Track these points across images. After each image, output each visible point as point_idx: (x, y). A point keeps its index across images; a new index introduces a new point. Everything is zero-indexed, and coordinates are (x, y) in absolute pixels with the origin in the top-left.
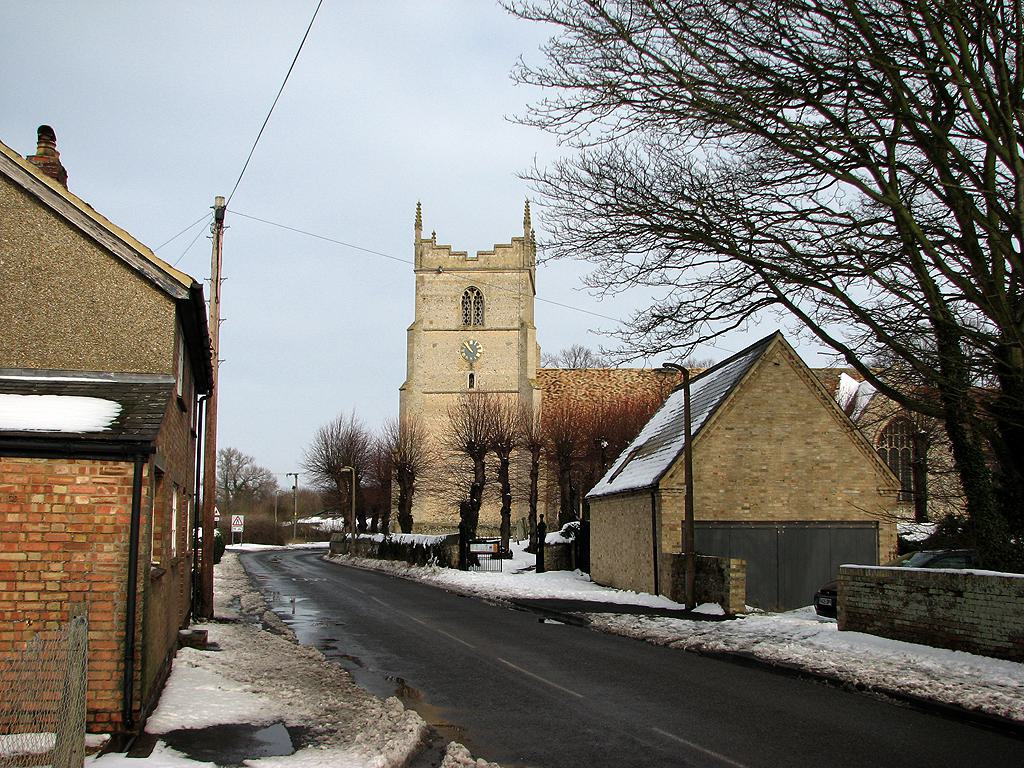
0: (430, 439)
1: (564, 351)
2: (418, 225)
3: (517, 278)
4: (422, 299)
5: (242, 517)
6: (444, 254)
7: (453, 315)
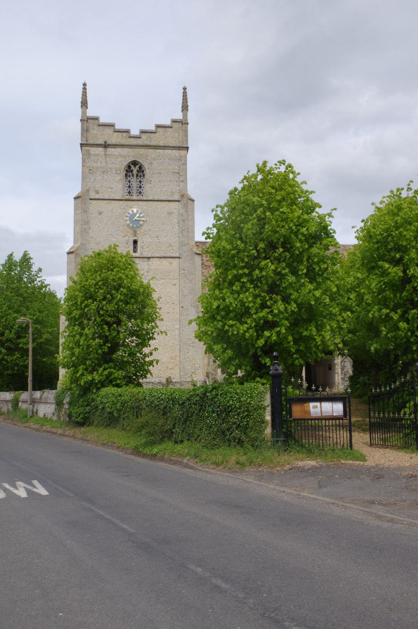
0: (149, 378)
1: (267, 162)
2: (84, 104)
3: (177, 155)
4: (88, 172)
5: (396, 319)
6: (109, 131)
7: (116, 185)
